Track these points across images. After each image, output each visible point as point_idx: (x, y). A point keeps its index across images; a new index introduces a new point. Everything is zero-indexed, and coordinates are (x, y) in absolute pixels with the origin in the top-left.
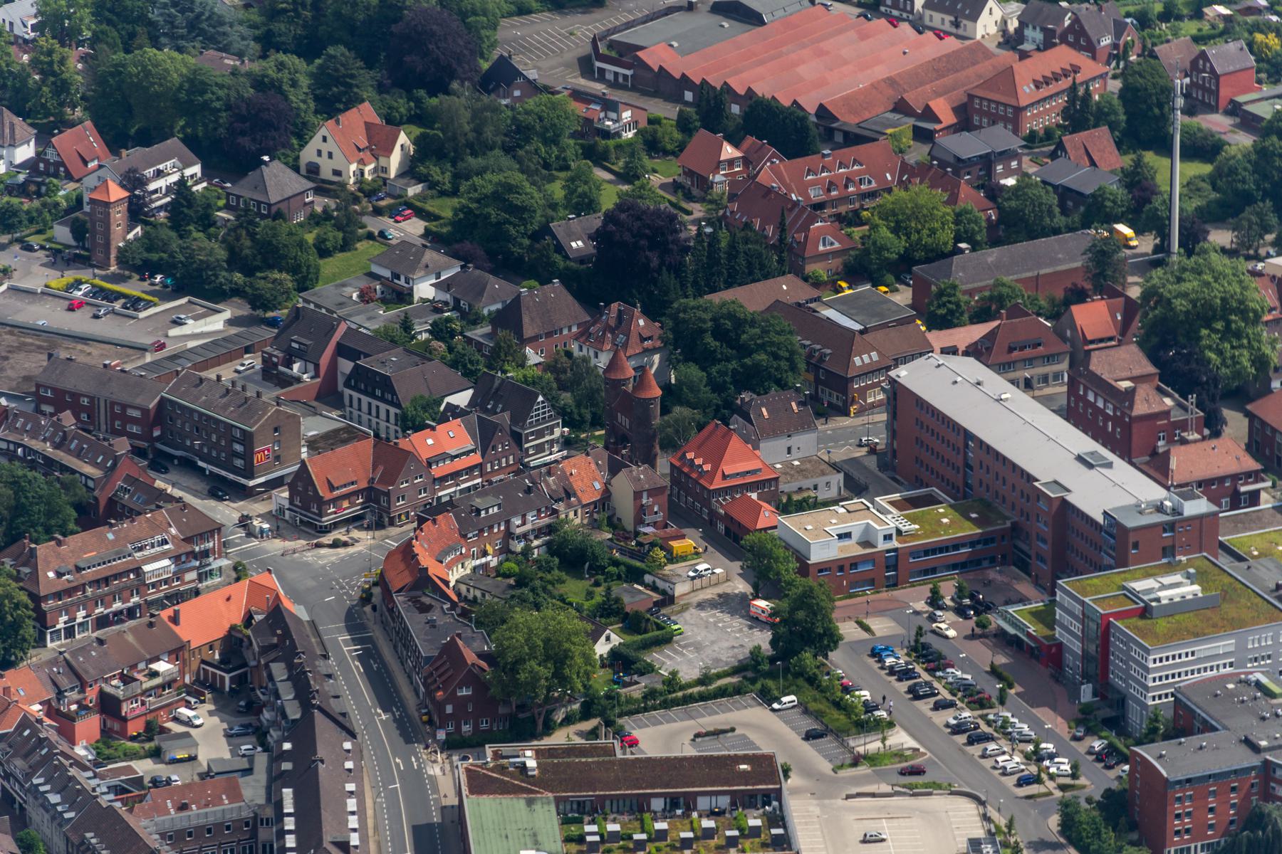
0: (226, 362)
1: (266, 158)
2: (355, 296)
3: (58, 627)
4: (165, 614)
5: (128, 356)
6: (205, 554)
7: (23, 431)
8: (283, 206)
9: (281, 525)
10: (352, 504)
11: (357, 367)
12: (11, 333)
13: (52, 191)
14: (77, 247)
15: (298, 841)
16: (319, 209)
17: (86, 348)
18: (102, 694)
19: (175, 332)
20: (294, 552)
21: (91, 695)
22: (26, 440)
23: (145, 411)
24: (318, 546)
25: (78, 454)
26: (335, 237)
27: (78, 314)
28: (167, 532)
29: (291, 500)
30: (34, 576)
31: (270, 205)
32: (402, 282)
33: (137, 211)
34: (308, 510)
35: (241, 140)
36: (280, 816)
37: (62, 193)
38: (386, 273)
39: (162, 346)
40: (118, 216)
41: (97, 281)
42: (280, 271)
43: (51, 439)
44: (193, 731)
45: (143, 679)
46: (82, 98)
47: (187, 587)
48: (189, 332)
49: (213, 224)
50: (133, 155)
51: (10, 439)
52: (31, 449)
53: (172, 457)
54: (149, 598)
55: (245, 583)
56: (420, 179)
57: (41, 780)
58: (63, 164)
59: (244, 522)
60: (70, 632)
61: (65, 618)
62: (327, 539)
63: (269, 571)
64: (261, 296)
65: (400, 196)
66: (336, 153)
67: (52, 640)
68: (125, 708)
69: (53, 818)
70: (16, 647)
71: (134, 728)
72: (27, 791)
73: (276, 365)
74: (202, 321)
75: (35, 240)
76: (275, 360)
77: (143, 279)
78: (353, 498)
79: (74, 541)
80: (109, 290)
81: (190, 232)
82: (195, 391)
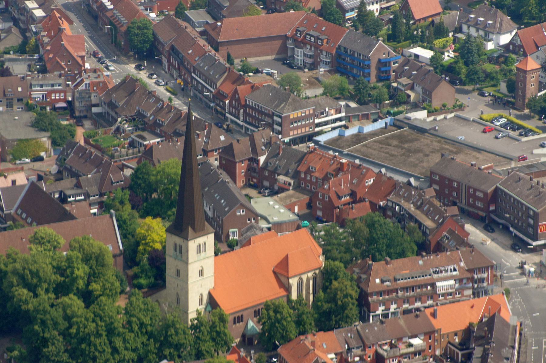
3: (378, 313)
12: (439, 142)
17: (478, 155)
18: (377, 354)
22: (403, 203)
23: (486, 194)
39: (525, 159)
51: (394, 200)
52: (403, 208)
53: (498, 224)
55: (485, 299)
70: (342, 321)
77: (540, 119)
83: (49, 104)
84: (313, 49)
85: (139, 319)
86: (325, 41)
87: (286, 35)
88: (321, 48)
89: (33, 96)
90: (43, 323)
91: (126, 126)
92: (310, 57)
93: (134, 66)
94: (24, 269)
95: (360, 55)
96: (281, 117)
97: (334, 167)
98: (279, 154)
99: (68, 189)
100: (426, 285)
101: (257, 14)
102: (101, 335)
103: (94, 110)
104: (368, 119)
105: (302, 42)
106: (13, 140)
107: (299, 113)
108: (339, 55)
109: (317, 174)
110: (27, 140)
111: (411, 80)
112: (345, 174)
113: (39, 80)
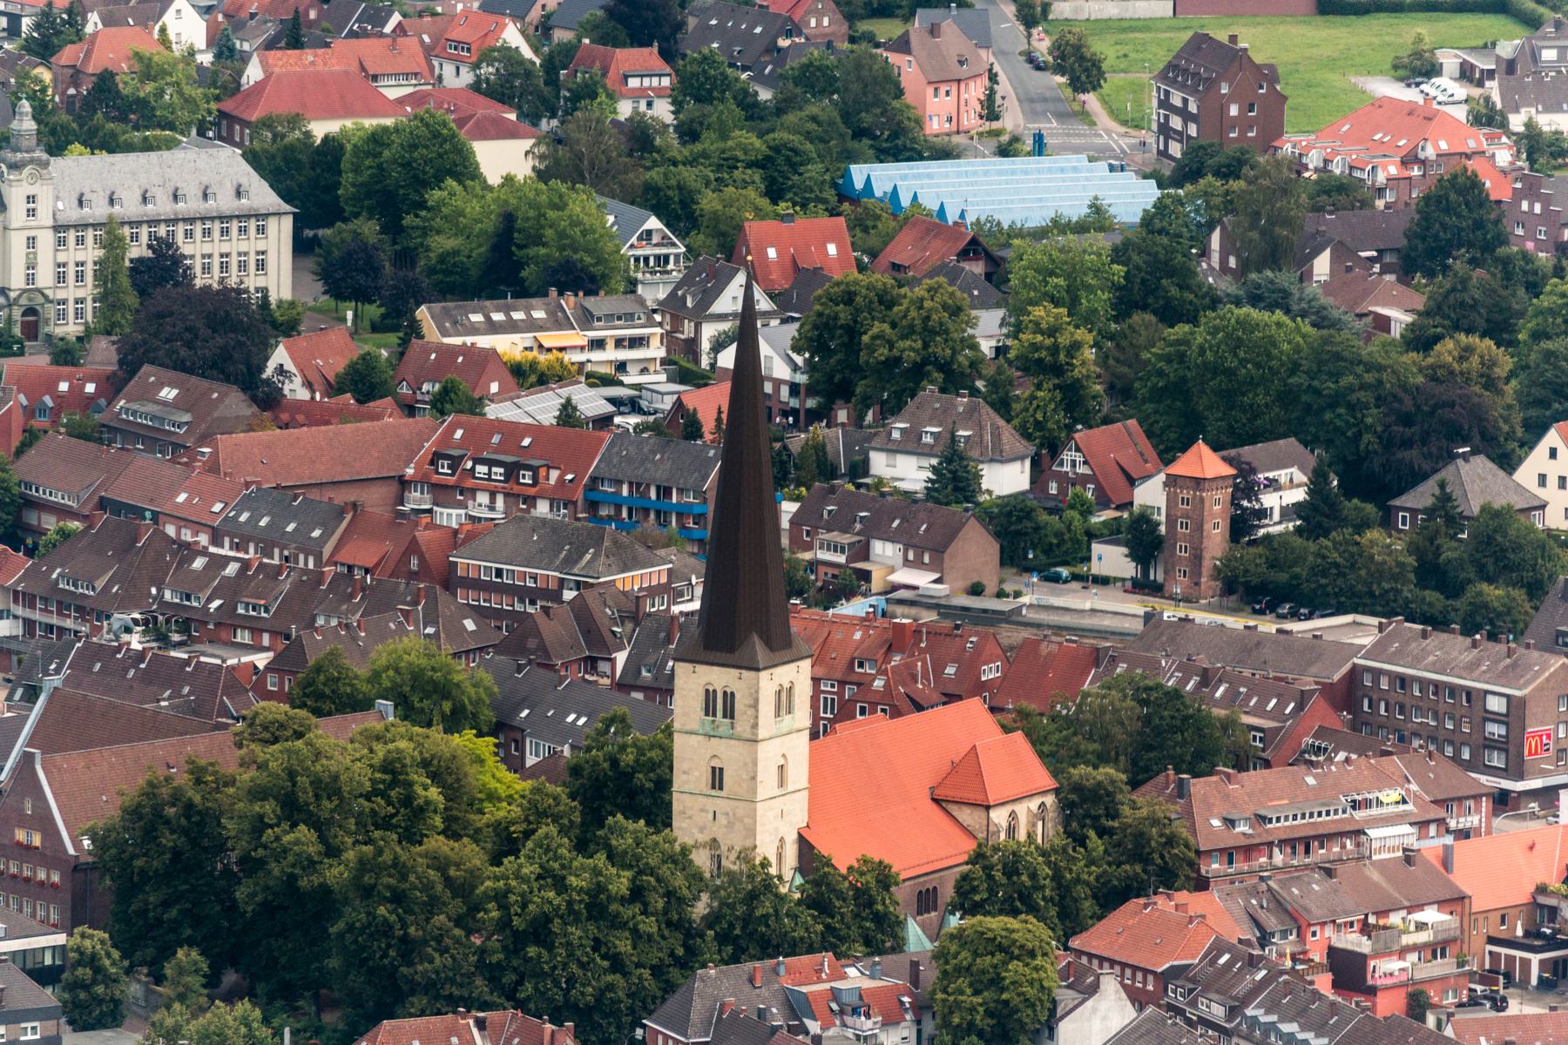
46: (1016, 337)
84: (500, 502)
90: (398, 898)
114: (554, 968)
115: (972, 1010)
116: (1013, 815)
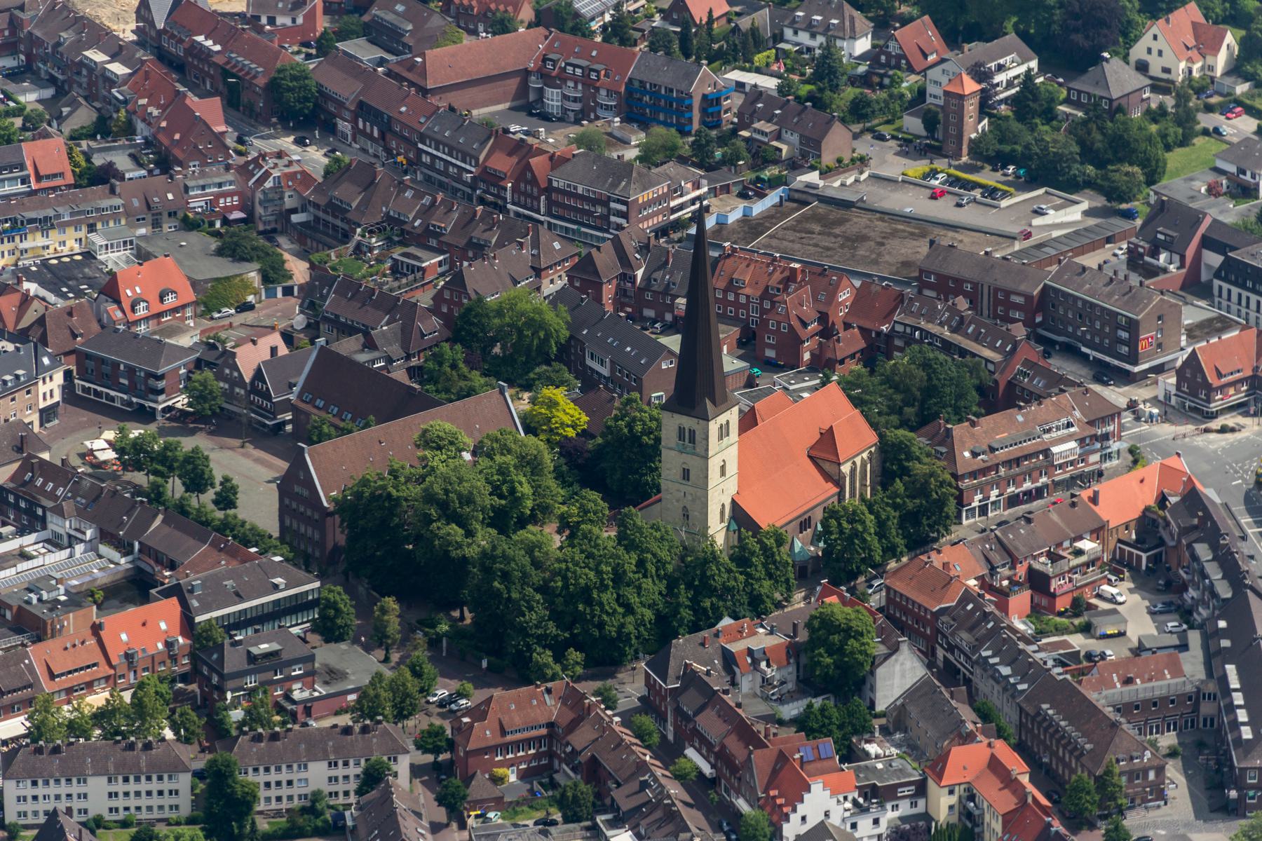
0: (1089, 251)
1: (1106, 55)
2: (1203, 190)
3: (974, 505)
4: (1085, 494)
5: (999, 244)
6: (1106, 437)
7: (919, 315)
8: (1123, 102)
9: (1170, 411)
10: (1238, 392)
11: (1228, 259)
12: (882, 220)
13: (896, 82)
14: (927, 138)
15: (1250, 714)
16: (1154, 106)
17: (956, 235)
18: (1031, 572)
19: (1037, 221)
20: (1184, 436)
21: (1021, 571)
22: (923, 324)
23: (1029, 298)
24: (1207, 431)
25: (976, 338)
26: (1175, 133)
27: (941, 202)
28: (1072, 416)
29: (1178, 387)
30: (951, 457)
31: (1111, 101)
32: (1248, 177)
33: (985, 108)
34: (1196, 396)
35: (1074, 37)
36: (1227, 691)
37: (905, 85)
38: (1232, 169)
40: (971, 107)
41: (952, 171)
42: (1131, 164)
43: (948, 322)
44: (1119, 608)
45: (1070, 557)
47: (1091, 468)
48: (1050, 222)
49: (1054, 117)
50: (975, 49)
52: (928, 333)
54: (1056, 479)
56: (1247, 78)
57: (989, 653)
58: (905, 57)
59: (1132, 405)
60: (983, 510)
61: (980, 496)
62: (1216, 424)
63: (1178, 455)
64: (1117, 189)
65: (1229, 94)
66: (1167, 51)
67: (967, 518)
68: (1054, 585)
69: (1005, 690)
70: (939, 524)
71: (1062, 604)
72: (973, 664)
73: (1142, 255)
74: (1062, 212)
75: (886, 130)
76: (1141, 250)
77: (995, 170)
78: (1239, 386)
79: (987, 422)
80: (965, 180)
81: (1036, 125)
82: (1078, 279)
83: (218, 215)
84: (580, 87)
85: (654, 555)
86: (603, 73)
87: (526, 69)
88: (598, 84)
89: (192, 205)
90: (506, 576)
91: (374, 240)
92: (575, 100)
93: (291, 138)
94: (446, 492)
95: (671, 90)
96: (625, 203)
97: (777, 276)
98: (667, 262)
99: (356, 352)
100: (1036, 454)
101: (454, 42)
102: (607, 587)
103: (295, 218)
104: (728, 192)
105: (559, 77)
106: (206, 281)
107: (649, 194)
108: (630, 91)
109: (748, 291)
110: (228, 278)
111: (775, 124)
112: (801, 287)
113: (196, 179)
114: (594, 616)
115: (828, 666)
116: (854, 463)
